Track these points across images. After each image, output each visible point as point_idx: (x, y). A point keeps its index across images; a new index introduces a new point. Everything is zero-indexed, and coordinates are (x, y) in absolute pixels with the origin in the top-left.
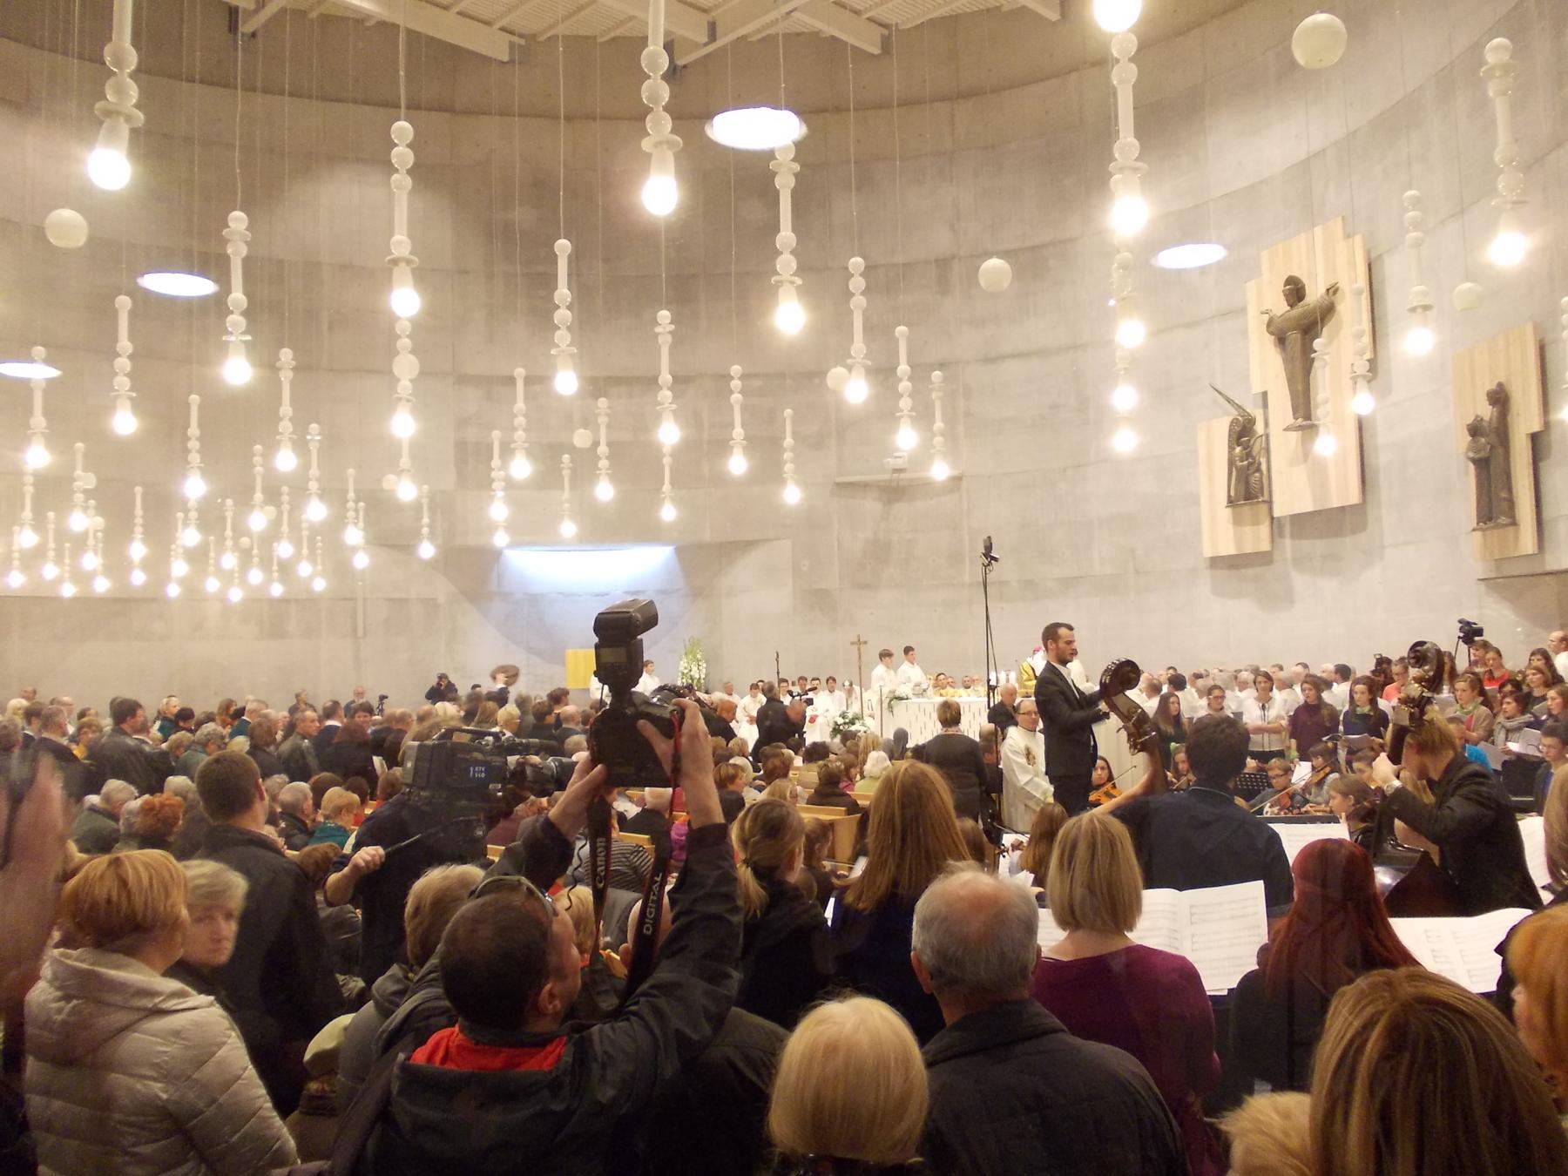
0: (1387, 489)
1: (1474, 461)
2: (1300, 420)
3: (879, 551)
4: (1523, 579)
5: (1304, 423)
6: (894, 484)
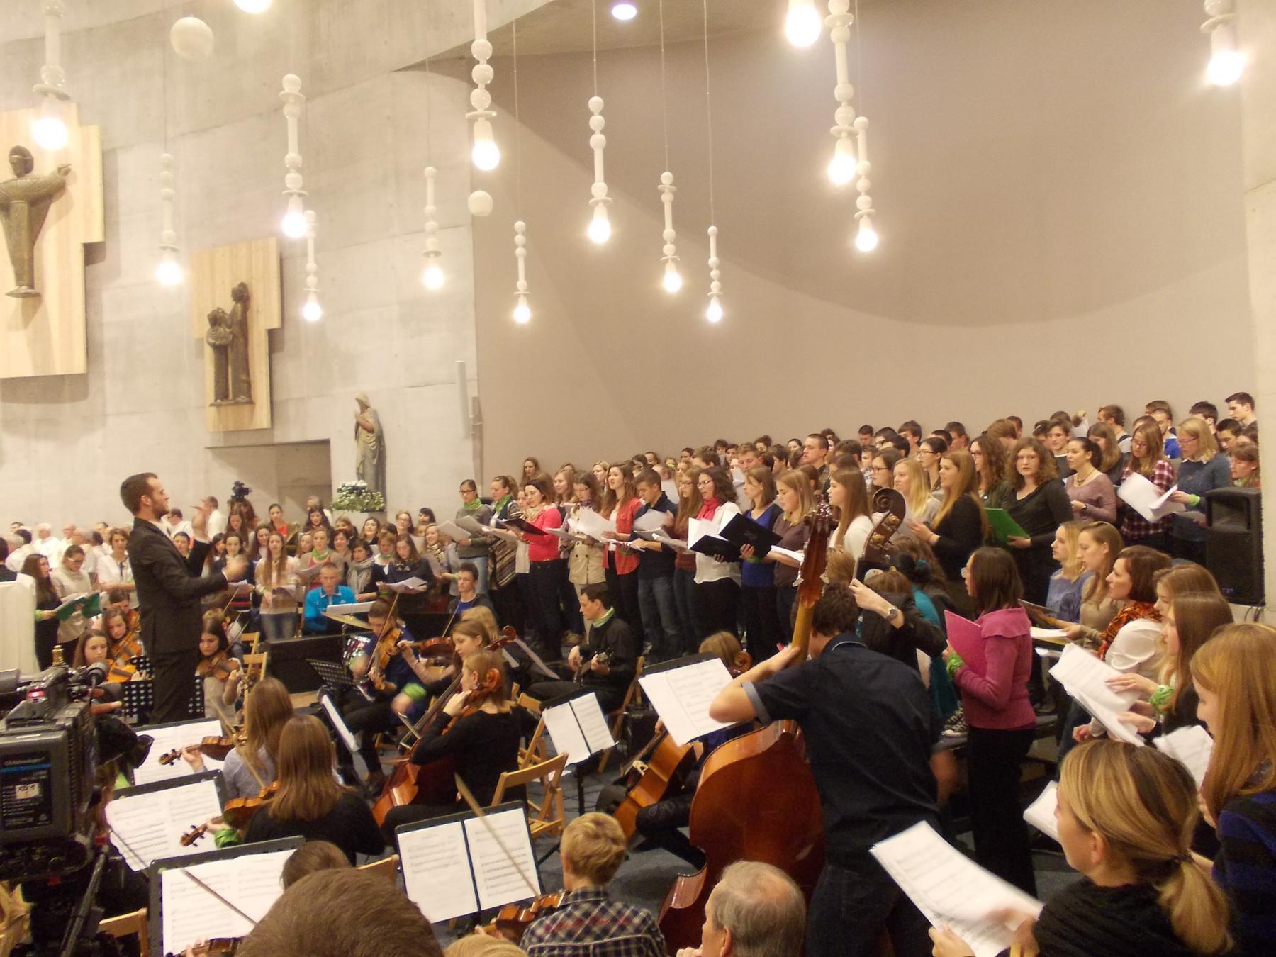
1: (216, 348)
5: (30, 291)
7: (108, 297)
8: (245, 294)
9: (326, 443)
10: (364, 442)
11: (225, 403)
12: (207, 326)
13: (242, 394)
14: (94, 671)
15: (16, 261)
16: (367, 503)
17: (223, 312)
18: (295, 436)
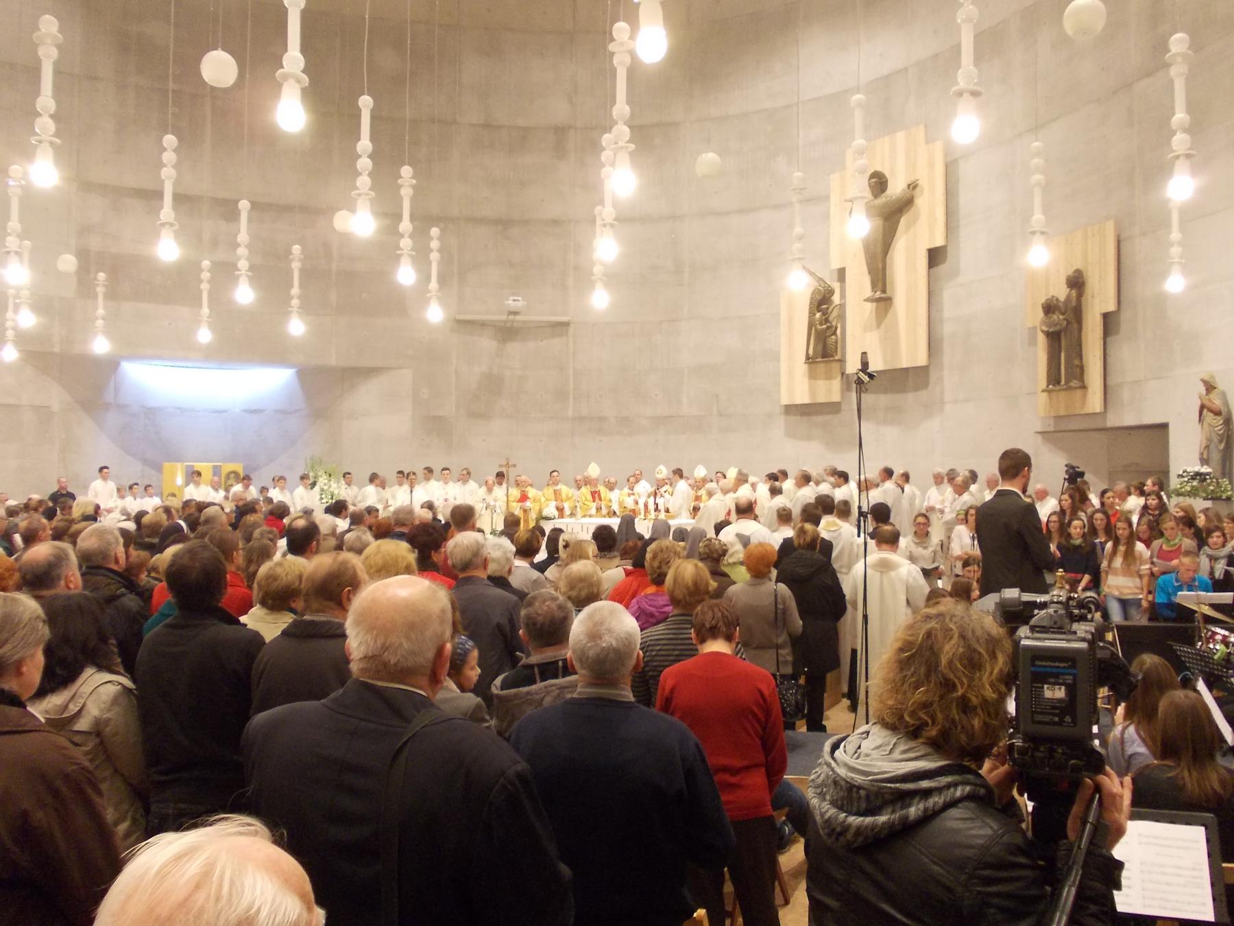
0: (949, 356)
2: (878, 293)
3: (493, 385)
4: (1093, 434)
5: (883, 295)
6: (508, 325)
7: (949, 294)
8: (1081, 280)
9: (1164, 427)
10: (1210, 425)
11: (1058, 388)
12: (1041, 314)
13: (1075, 378)
14: (1090, 599)
15: (871, 271)
16: (1212, 491)
17: (1057, 299)
18: (1129, 420)
